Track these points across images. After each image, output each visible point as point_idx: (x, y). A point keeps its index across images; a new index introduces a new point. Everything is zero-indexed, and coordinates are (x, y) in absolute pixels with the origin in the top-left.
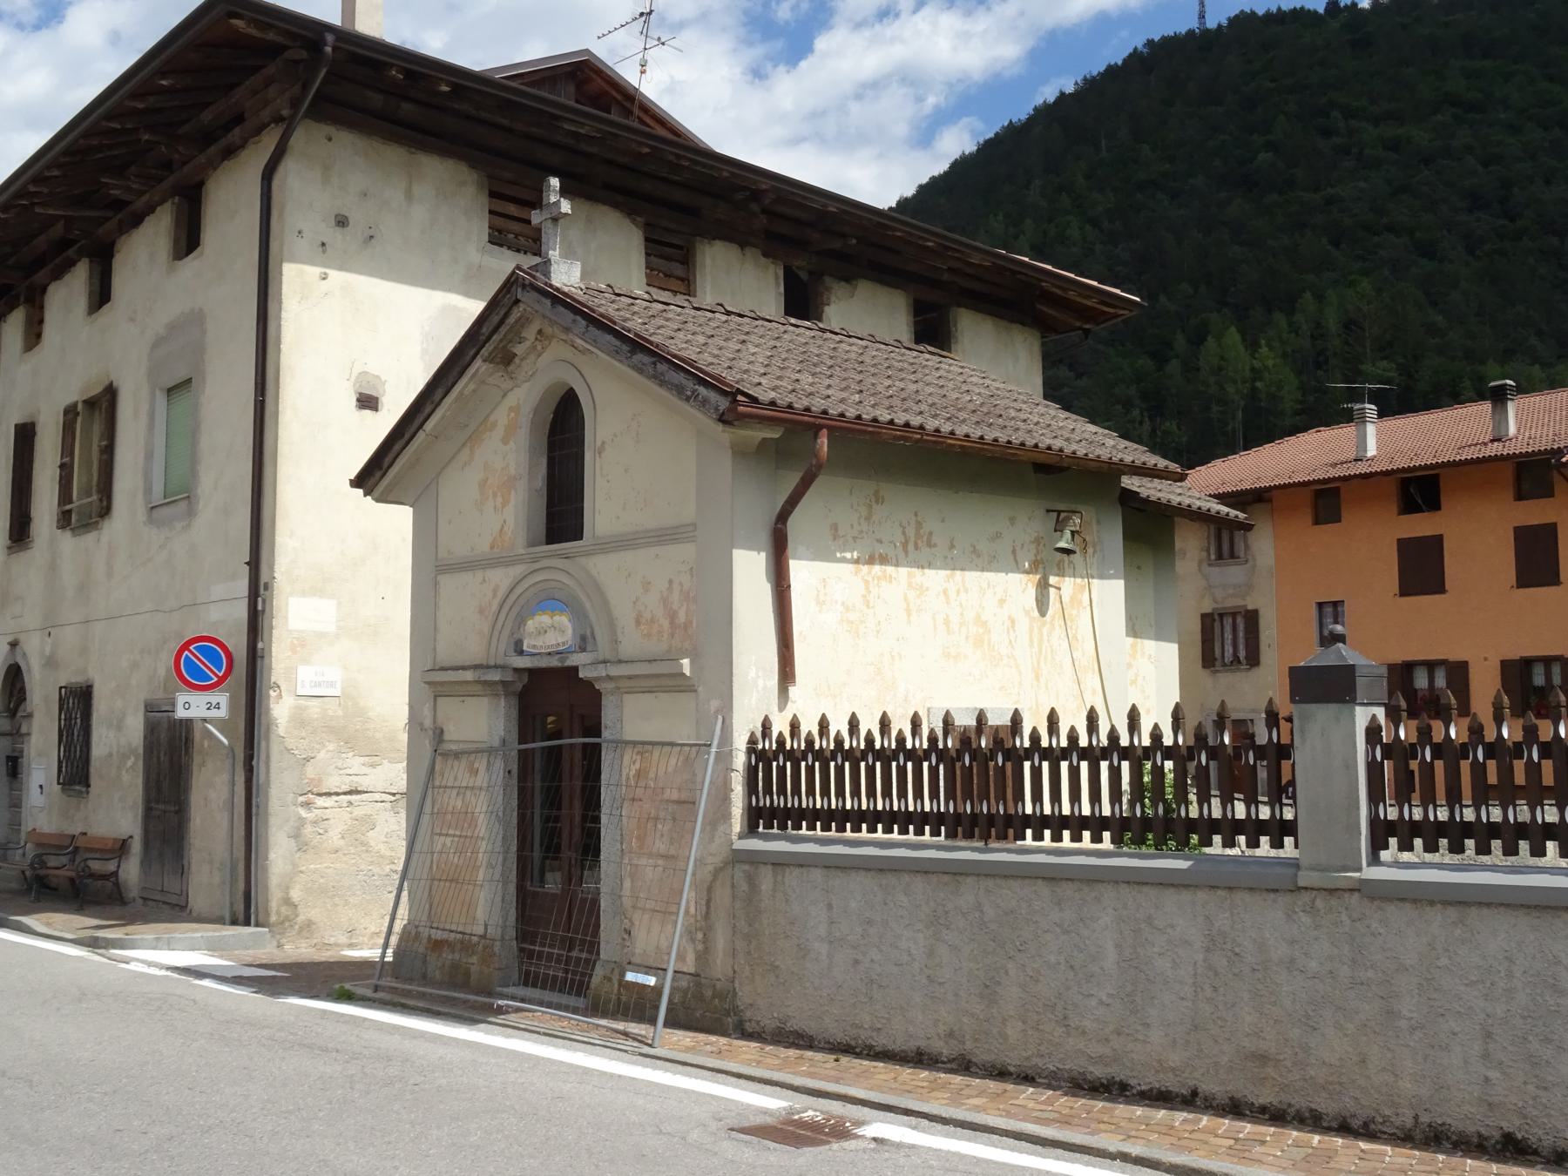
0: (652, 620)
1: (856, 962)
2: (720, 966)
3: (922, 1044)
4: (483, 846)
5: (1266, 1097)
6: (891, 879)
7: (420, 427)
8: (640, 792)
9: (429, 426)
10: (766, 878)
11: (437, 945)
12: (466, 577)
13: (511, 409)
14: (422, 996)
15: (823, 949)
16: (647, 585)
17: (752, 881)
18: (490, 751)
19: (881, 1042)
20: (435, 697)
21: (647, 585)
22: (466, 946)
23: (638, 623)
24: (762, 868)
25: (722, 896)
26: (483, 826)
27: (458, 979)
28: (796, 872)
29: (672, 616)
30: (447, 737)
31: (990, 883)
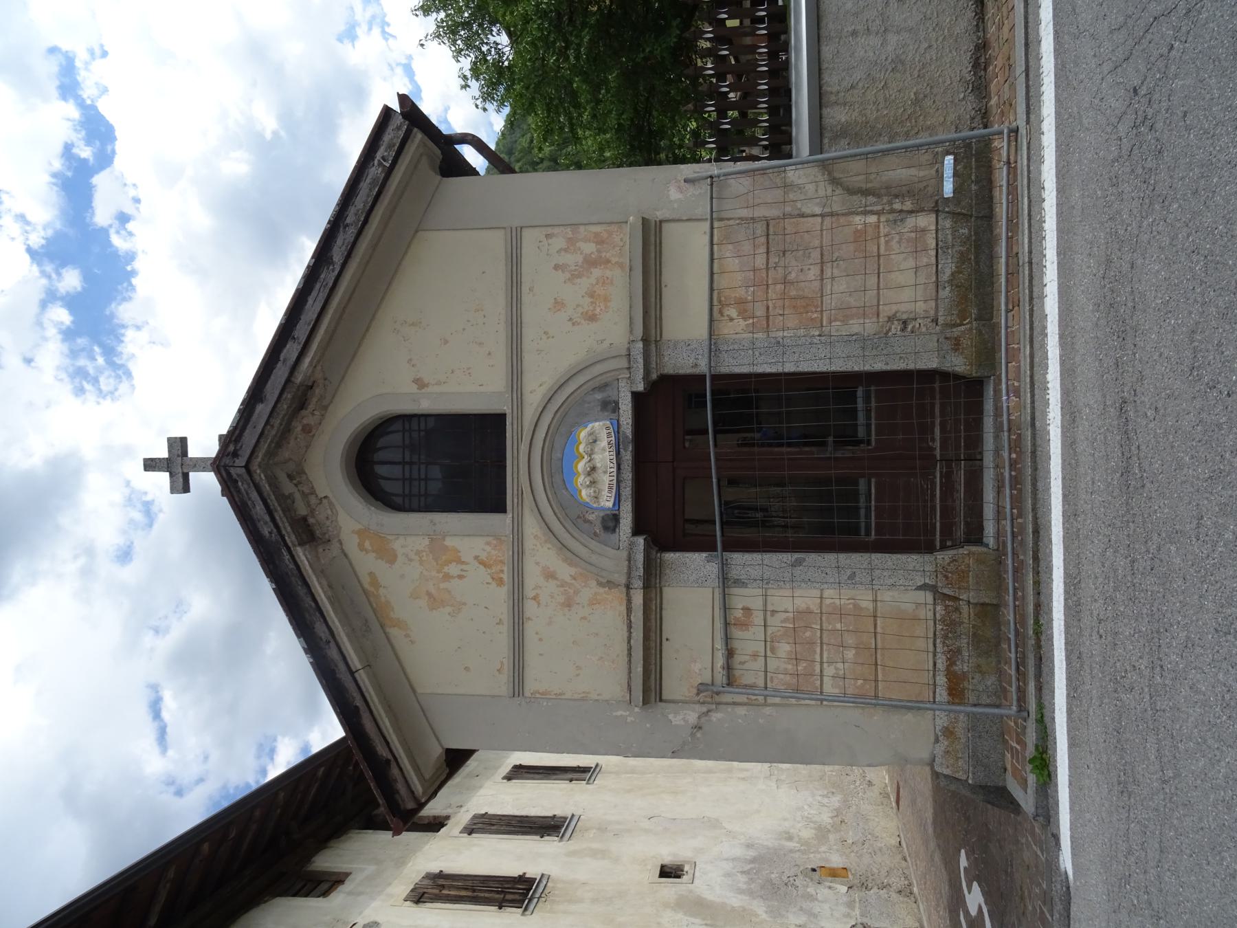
0: (592, 294)
7: (352, 673)
9: (355, 662)
10: (837, 116)
11: (956, 692)
12: (530, 629)
13: (361, 547)
14: (1021, 675)
15: (893, 39)
17: (844, 132)
18: (726, 581)
20: (661, 700)
21: (559, 305)
22: (950, 626)
23: (592, 318)
24: (827, 121)
26: (806, 598)
28: (826, 77)
29: (591, 263)
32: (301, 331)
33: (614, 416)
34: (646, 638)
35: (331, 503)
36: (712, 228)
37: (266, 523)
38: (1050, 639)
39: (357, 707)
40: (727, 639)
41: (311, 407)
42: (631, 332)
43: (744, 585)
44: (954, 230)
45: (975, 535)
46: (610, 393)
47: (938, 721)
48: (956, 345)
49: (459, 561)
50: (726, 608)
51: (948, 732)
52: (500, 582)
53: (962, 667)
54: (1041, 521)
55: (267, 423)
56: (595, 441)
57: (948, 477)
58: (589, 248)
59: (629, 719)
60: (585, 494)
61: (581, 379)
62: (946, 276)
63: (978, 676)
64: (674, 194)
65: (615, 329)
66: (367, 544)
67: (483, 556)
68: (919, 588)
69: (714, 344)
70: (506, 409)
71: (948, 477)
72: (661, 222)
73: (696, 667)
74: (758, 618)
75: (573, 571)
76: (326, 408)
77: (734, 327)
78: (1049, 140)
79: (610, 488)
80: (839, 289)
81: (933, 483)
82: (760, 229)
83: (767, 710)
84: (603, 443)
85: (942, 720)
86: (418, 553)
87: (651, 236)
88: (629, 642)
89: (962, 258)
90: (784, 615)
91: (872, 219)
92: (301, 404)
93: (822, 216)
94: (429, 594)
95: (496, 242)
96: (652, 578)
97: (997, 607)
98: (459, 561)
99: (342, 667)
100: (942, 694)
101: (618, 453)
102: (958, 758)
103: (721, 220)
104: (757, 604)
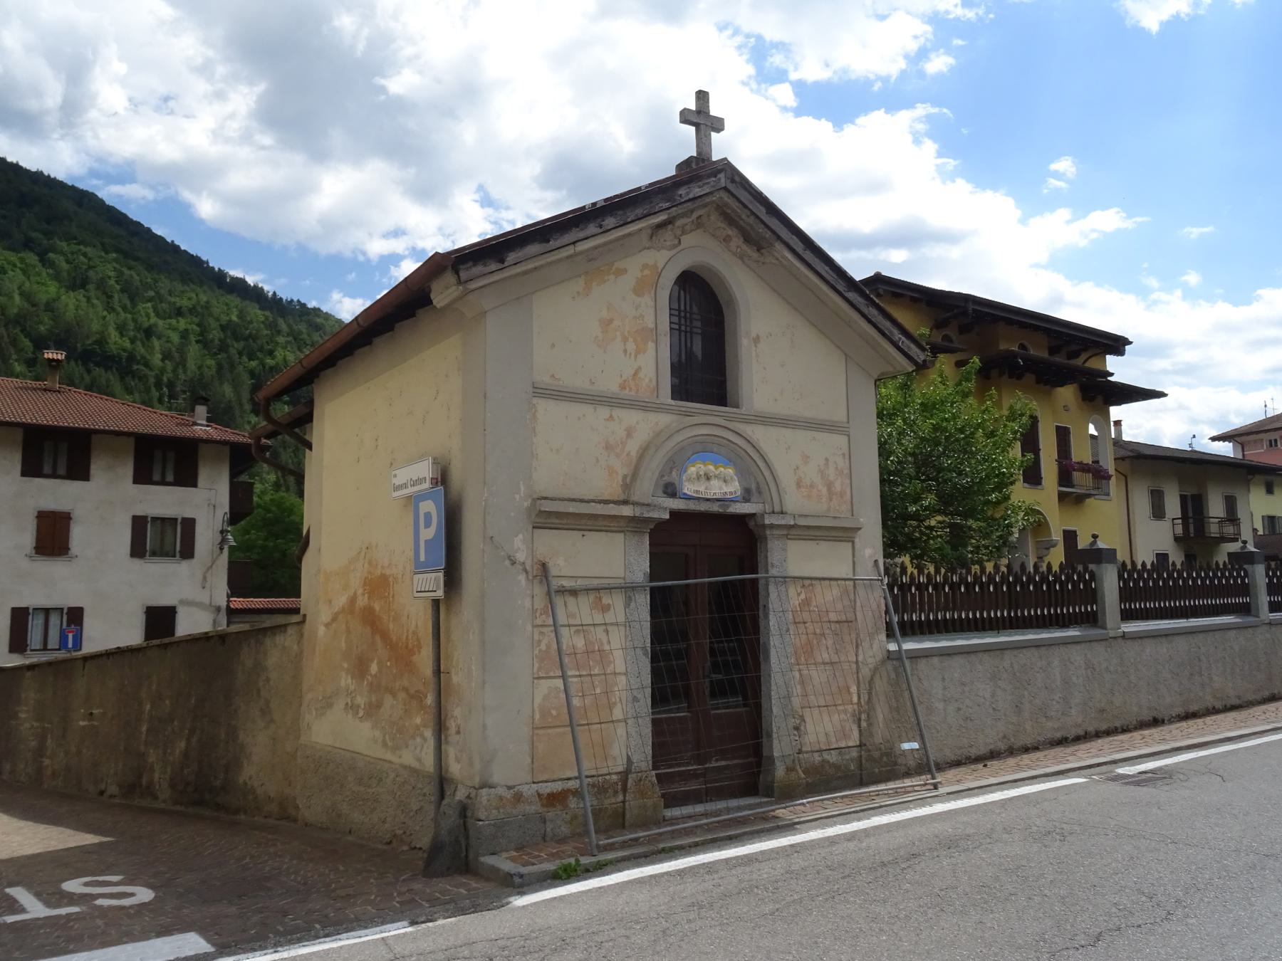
0: (812, 486)
1: (959, 709)
2: (880, 734)
3: (992, 747)
4: (622, 680)
5: (1104, 727)
6: (973, 657)
8: (806, 616)
9: (582, 247)
11: (554, 799)
12: (587, 409)
13: (645, 266)
14: (624, 845)
15: (940, 706)
16: (806, 459)
18: (629, 589)
19: (974, 752)
21: (806, 459)
22: (601, 789)
23: (799, 485)
25: (881, 686)
26: (619, 662)
27: (616, 821)
28: (924, 661)
29: (830, 486)
30: (553, 571)
31: (1016, 652)
32: (808, 256)
33: (740, 499)
34: (594, 517)
35: (675, 246)
36: (845, 580)
37: (688, 194)
38: (661, 861)
39: (548, 241)
40: (587, 590)
41: (744, 247)
42: (801, 516)
43: (627, 605)
44: (852, 760)
45: (672, 800)
46: (755, 498)
47: (527, 787)
48: (790, 769)
49: (638, 352)
50: (610, 589)
51: (518, 798)
52: (623, 387)
53: (573, 803)
54: (609, 868)
55: (753, 213)
56: (725, 481)
57: (693, 775)
58: (838, 487)
59: (517, 497)
60: (693, 470)
61: (767, 473)
62: (826, 756)
63: (568, 817)
64: (868, 552)
65: (796, 502)
66: (647, 272)
67: (641, 375)
68: (629, 759)
69: (785, 579)
70: (743, 411)
71: (693, 775)
72: (853, 542)
73: (561, 562)
74: (598, 618)
75: (634, 454)
76: (741, 258)
77: (795, 596)
78: (939, 808)
79: (697, 492)
80: (818, 676)
81: (688, 764)
82: (850, 616)
83: (529, 628)
84: (726, 489)
85: (529, 790)
86: (642, 316)
87: (845, 534)
88: (593, 501)
89: (836, 766)
90: (605, 641)
91: (855, 699)
92: (747, 238)
93: (857, 662)
94: (611, 321)
95: (839, 415)
96: (634, 524)
97: (623, 826)
98: (638, 352)
99: (582, 235)
100: (547, 789)
101: (718, 500)
102: (497, 809)
103: (855, 586)
104: (610, 617)
